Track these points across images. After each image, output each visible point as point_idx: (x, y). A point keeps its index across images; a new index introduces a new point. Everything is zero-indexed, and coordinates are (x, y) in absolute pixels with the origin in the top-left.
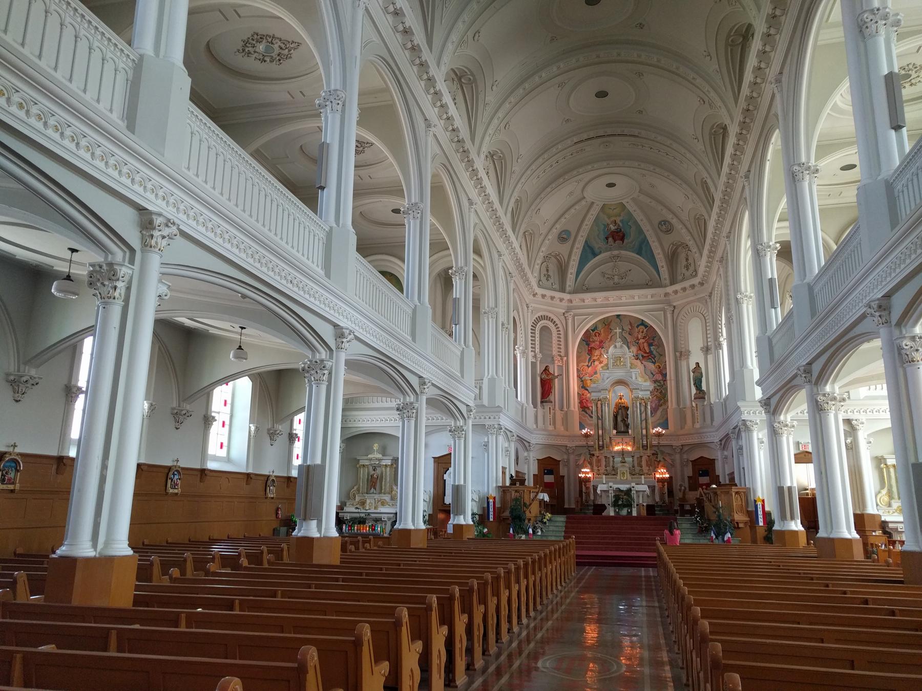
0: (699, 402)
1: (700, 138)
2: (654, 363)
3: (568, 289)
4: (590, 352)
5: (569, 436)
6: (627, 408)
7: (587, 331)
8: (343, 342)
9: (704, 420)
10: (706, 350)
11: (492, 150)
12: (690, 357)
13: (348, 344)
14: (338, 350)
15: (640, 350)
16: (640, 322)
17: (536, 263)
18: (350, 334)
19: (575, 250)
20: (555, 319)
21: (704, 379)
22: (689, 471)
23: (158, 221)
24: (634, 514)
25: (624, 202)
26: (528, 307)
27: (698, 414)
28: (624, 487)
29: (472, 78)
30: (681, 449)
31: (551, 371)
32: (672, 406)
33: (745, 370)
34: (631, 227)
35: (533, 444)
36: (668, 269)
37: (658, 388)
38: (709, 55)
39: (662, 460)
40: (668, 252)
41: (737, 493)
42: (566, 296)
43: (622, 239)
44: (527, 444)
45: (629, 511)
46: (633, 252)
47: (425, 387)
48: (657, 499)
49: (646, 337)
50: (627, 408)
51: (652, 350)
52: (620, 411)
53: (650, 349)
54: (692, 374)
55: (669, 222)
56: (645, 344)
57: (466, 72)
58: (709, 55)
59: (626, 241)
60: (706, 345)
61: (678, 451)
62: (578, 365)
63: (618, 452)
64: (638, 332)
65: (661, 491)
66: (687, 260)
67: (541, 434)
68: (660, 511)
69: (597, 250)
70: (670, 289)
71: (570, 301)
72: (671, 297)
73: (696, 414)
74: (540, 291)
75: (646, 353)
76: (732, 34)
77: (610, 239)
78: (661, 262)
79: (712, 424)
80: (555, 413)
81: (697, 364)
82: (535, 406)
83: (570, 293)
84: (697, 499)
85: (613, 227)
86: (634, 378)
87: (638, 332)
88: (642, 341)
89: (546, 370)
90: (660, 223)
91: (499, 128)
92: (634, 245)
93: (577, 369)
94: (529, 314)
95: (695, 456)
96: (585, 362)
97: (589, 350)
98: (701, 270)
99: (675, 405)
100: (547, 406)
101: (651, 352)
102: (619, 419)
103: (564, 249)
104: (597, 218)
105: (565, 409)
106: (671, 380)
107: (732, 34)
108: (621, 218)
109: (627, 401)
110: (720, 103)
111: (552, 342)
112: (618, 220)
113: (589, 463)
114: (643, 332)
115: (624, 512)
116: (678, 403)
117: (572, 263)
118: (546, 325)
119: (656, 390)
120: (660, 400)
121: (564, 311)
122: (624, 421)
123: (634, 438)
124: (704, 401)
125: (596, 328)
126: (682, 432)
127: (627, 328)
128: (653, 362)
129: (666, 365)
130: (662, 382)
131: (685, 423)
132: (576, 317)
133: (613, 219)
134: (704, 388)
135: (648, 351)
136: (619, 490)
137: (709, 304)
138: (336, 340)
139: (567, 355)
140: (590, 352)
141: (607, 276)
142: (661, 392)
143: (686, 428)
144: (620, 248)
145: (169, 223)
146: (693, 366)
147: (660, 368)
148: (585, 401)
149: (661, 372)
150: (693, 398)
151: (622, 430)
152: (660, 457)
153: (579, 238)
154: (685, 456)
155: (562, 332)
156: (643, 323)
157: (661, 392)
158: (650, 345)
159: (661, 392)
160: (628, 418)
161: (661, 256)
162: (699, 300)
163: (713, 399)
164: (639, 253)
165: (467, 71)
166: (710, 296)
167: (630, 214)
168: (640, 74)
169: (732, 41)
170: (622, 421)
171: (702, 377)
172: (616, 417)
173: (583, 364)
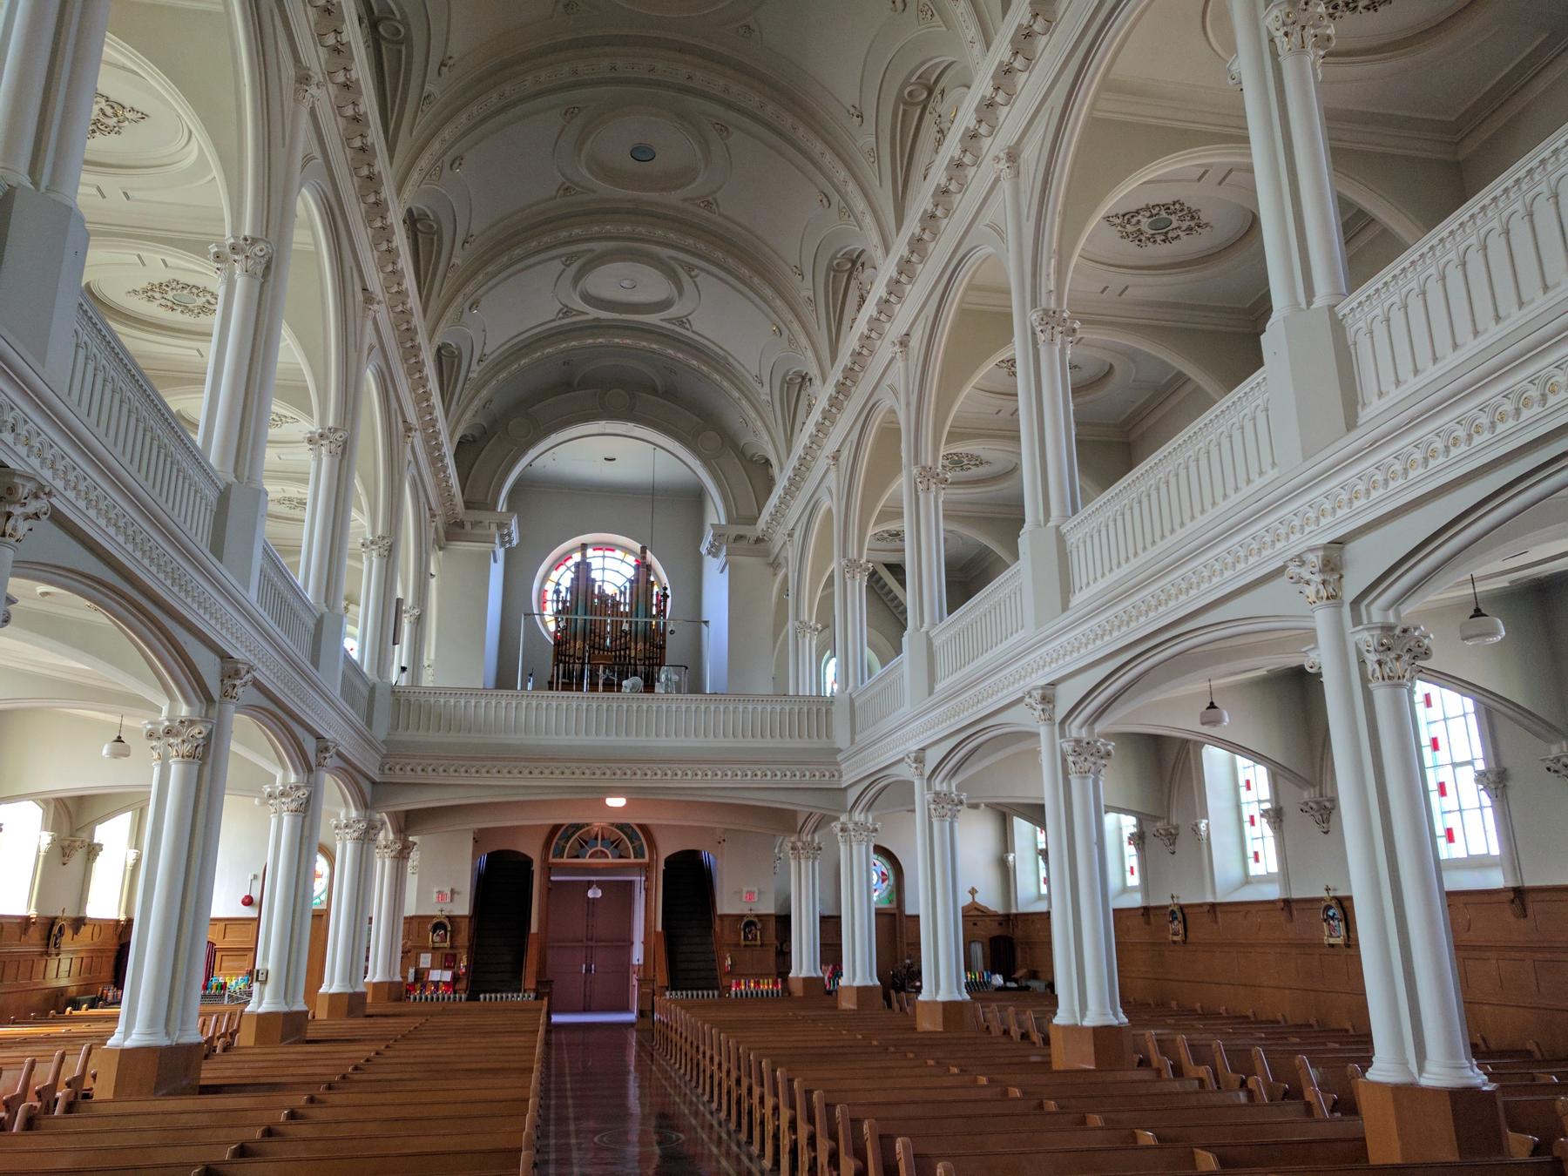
1: (766, 380)
8: (234, 686)
11: (417, 208)
13: (242, 689)
14: (225, 699)
18: (37, 497)
23: (24, 489)
29: (435, 226)
38: (860, 116)
44: (310, 745)
47: (238, 682)
57: (394, 14)
58: (860, 116)
76: (839, 256)
91: (439, 163)
107: (839, 256)
110: (804, 341)
138: (222, 681)
145: (41, 491)
165: (396, 12)
168: (723, 129)
169: (838, 264)
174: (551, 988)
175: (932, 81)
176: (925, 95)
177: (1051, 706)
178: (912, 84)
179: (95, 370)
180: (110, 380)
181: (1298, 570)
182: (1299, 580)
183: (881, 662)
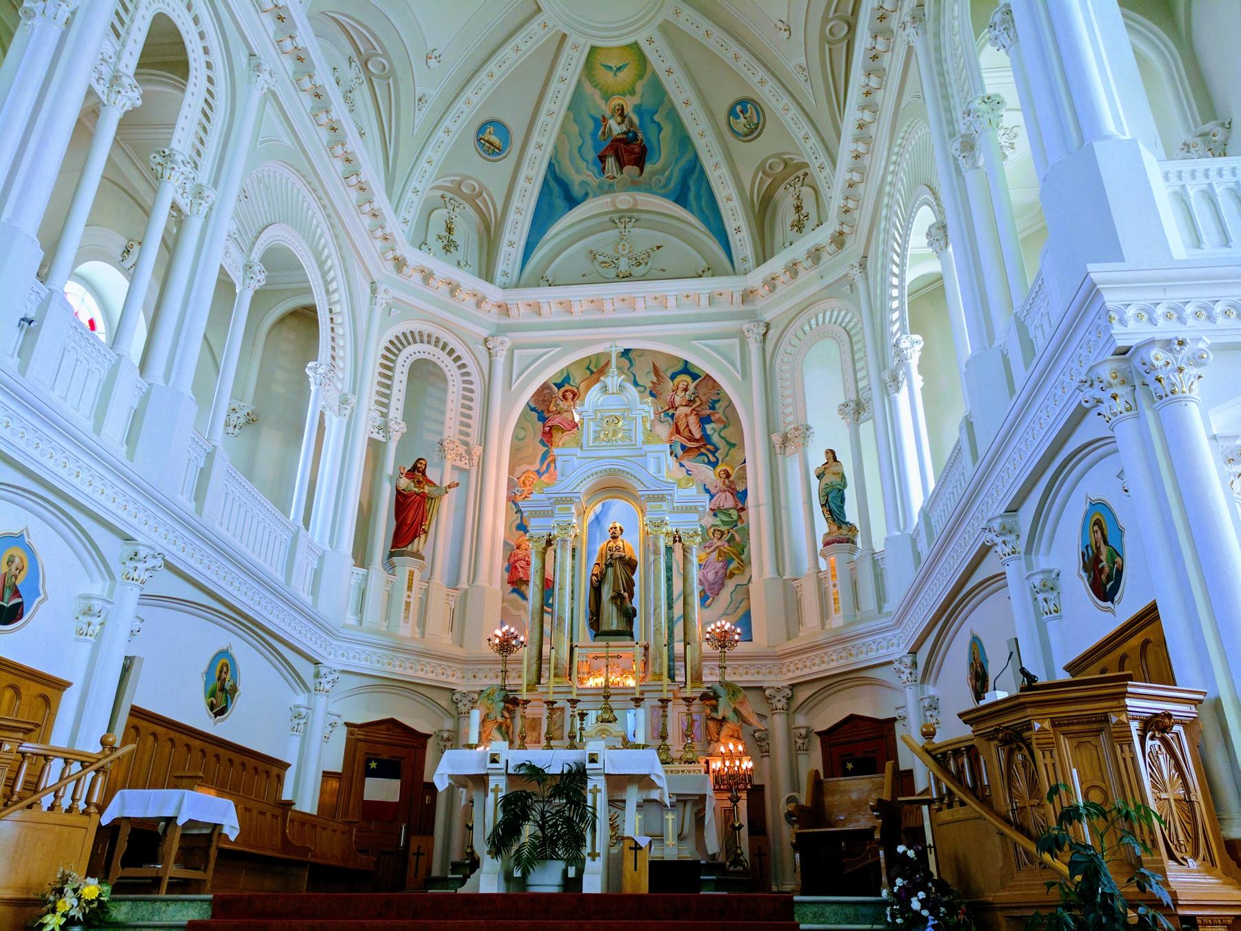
0: (838, 556)
2: (714, 465)
3: (499, 277)
4: (548, 436)
5: (464, 662)
6: (631, 565)
7: (545, 386)
9: (857, 605)
10: (856, 409)
12: (810, 444)
15: (678, 432)
16: (680, 367)
17: (410, 188)
19: (521, 183)
20: (460, 350)
21: (850, 493)
22: (813, 761)
24: (593, 883)
25: (642, 38)
26: (374, 291)
27: (838, 590)
28: (555, 760)
30: (789, 699)
31: (430, 474)
32: (761, 573)
33: (1098, 146)
34: (660, 129)
35: (332, 671)
36: (752, 234)
37: (724, 528)
38: (788, 30)
39: (730, 715)
40: (752, 197)
41: (1156, 724)
42: (493, 293)
43: (640, 160)
45: (572, 873)
46: (664, 196)
48: (713, 844)
49: (693, 401)
50: (631, 565)
51: (709, 432)
52: (610, 570)
53: (704, 430)
54: (815, 483)
55: (753, 102)
56: (692, 420)
58: (788, 30)
59: (648, 167)
60: (854, 397)
61: (780, 705)
62: (512, 470)
63: (595, 692)
64: (675, 391)
65: (726, 820)
66: (798, 208)
67: (371, 645)
68: (718, 885)
69: (577, 191)
70: (756, 277)
71: (504, 309)
72: (759, 305)
73: (832, 590)
74: (415, 258)
75: (691, 439)
77: (611, 162)
78: (735, 218)
79: (880, 609)
80: (427, 591)
81: (832, 455)
82: (361, 556)
83: (504, 287)
84: (881, 806)
85: (616, 128)
86: (652, 470)
87: (675, 391)
88: (683, 410)
89: (416, 471)
90: (732, 112)
92: (669, 179)
93: (510, 480)
94: (378, 310)
95: (831, 714)
96: (532, 463)
97: (544, 433)
98: (835, 200)
99: (769, 571)
100: (405, 565)
101: (706, 438)
102: (607, 593)
103: (492, 175)
104: (575, 104)
105: (464, 584)
106: (758, 506)
108: (636, 100)
109: (632, 544)
111: (443, 413)
112: (630, 104)
113: (500, 727)
114: (686, 390)
115: (547, 879)
116: (779, 569)
117: (512, 216)
118: (426, 356)
119: (718, 535)
120: (727, 562)
121: (485, 333)
122: (622, 599)
123: (646, 648)
124: (852, 551)
125: (567, 380)
126: (794, 644)
127: (647, 380)
128: (709, 463)
129: (744, 469)
130: (734, 513)
131: (800, 621)
132: (516, 352)
133: (616, 101)
134: (851, 513)
135: (697, 436)
136: (535, 773)
137: (861, 286)
139: (484, 440)
140: (548, 436)
141: (601, 259)
142: (732, 538)
143: (801, 634)
144: (635, 185)
146: (817, 460)
147: (728, 476)
148: (523, 563)
149: (734, 492)
150: (820, 546)
151: (614, 627)
152: (724, 708)
153: (531, 150)
154: (800, 720)
155: (475, 377)
156: (686, 369)
157: (731, 540)
158: (704, 420)
159: (731, 540)
160: (631, 595)
161: (736, 203)
162: (832, 291)
163: (879, 536)
164: (681, 199)
166: (863, 266)
167: (657, 88)
170: (613, 598)
171: (845, 486)
172: (596, 590)
173: (524, 467)
174: (717, 701)
175: (850, 12)
176: (846, 29)
177: (1055, 594)
178: (832, 19)
179: (227, 494)
180: (230, 492)
181: (899, 665)
182: (899, 671)
183: (1117, 261)
